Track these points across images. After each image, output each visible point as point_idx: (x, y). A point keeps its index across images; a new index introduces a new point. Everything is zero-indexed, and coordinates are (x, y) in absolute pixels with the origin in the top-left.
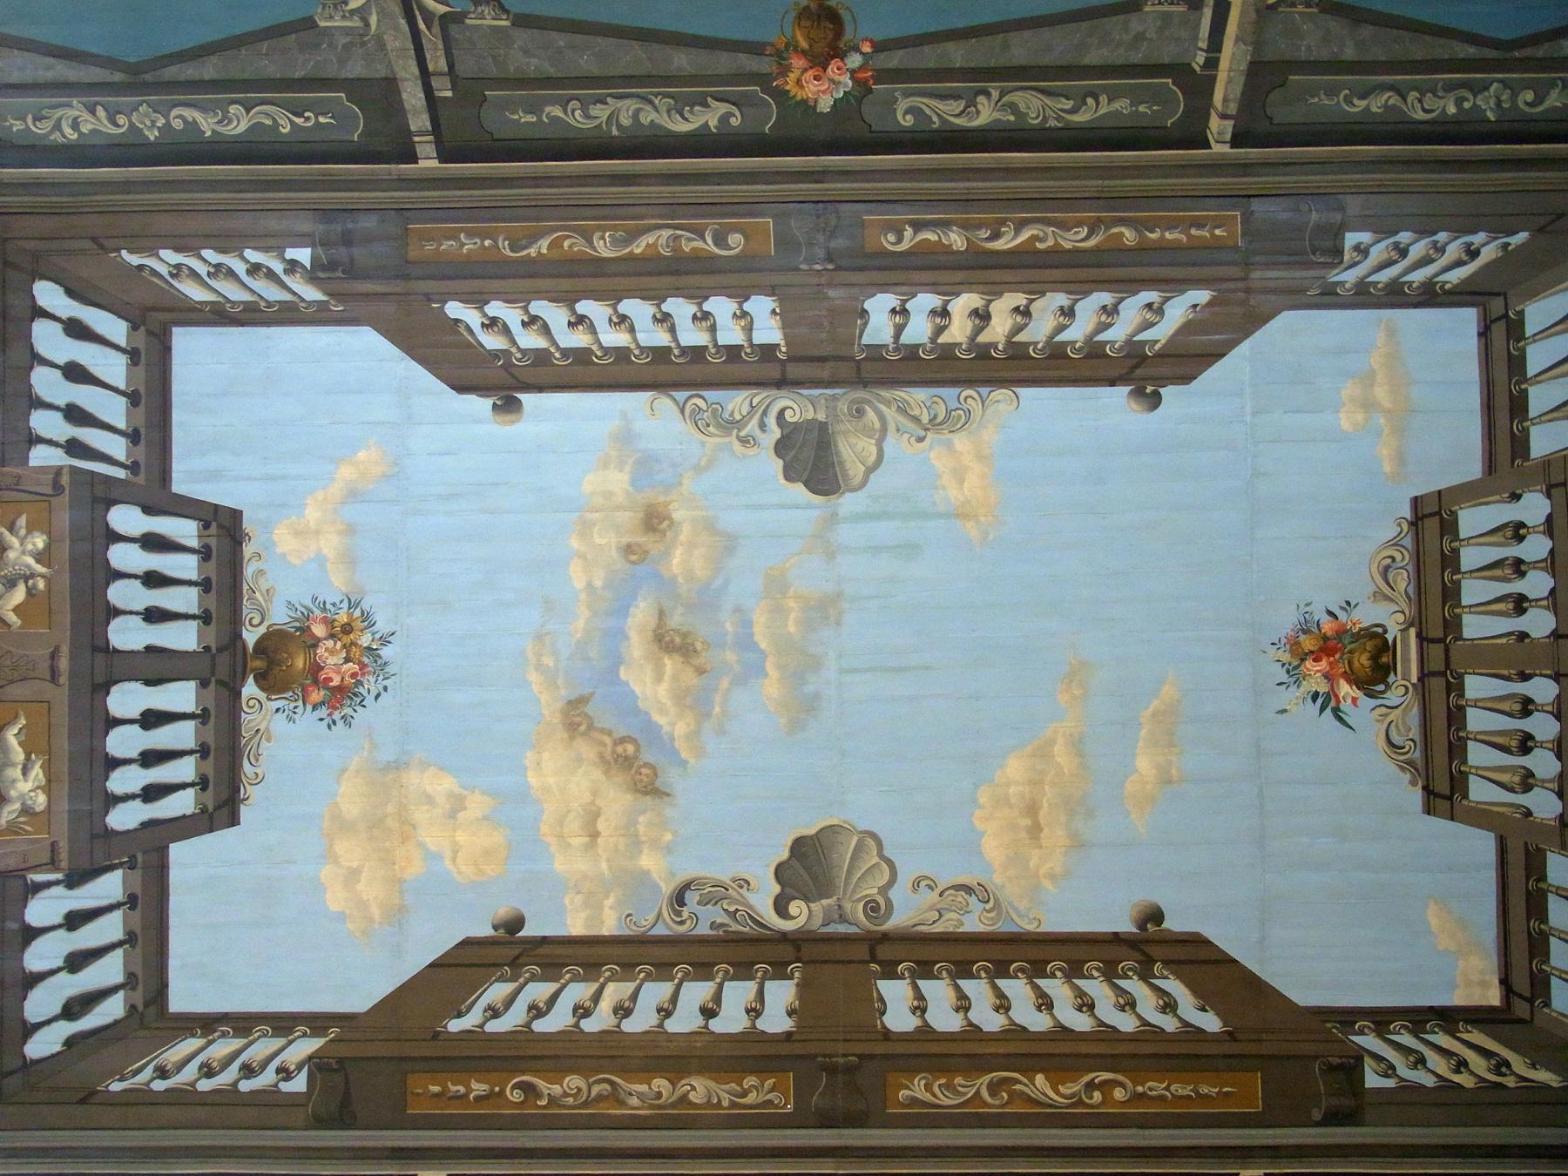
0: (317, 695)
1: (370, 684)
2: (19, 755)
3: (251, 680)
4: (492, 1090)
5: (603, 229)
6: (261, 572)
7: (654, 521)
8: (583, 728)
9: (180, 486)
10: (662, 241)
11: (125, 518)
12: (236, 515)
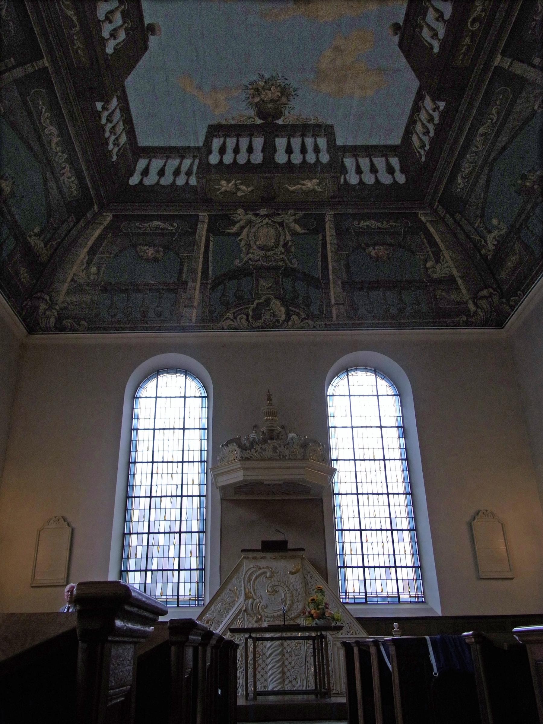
0: (284, 100)
1: (280, 82)
2: (299, 186)
3: (277, 121)
11: (214, 159)
12: (210, 127)
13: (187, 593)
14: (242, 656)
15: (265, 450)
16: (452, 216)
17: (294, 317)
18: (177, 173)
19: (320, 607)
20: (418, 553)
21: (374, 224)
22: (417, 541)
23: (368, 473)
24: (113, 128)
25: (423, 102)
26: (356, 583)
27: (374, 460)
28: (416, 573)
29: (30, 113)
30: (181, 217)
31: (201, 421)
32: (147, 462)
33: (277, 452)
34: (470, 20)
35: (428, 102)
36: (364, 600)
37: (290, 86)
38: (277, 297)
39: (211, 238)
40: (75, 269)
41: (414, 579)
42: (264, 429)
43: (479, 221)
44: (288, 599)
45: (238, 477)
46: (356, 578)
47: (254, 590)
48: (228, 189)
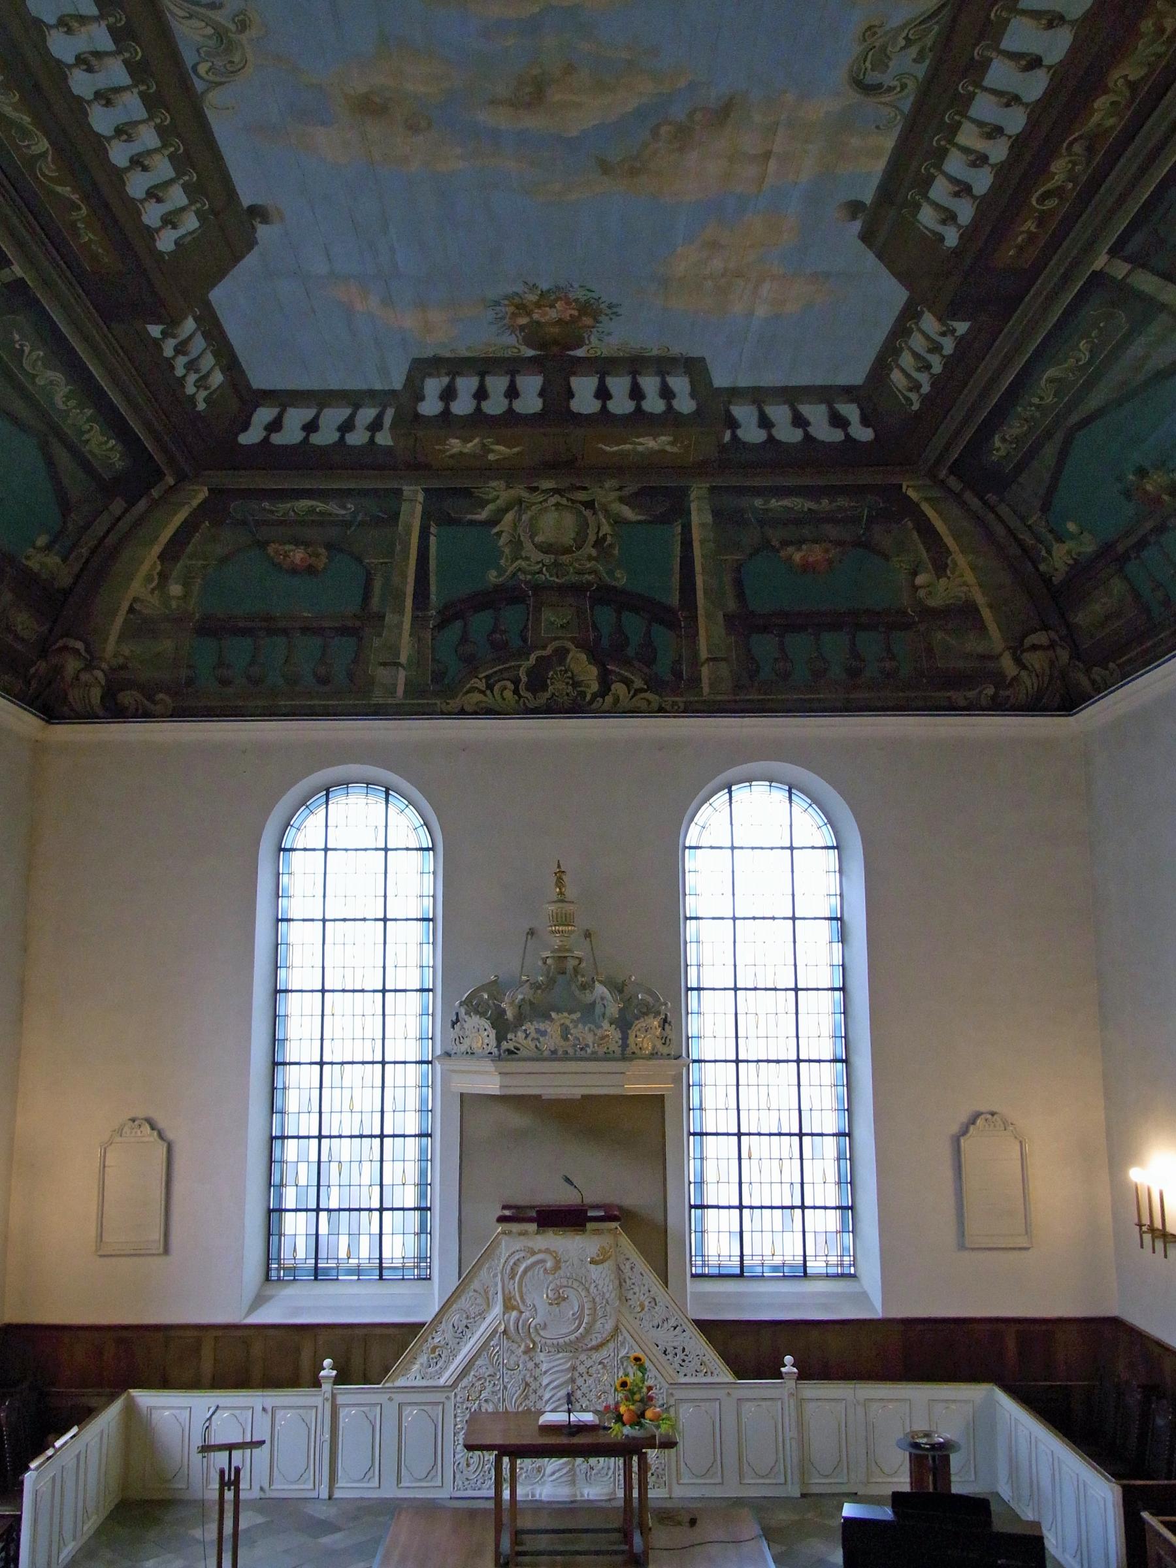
2: (628, 447)
11: (430, 406)
13: (398, 1254)
15: (544, 1033)
17: (619, 688)
19: (637, 1397)
20: (849, 1181)
22: (848, 1157)
23: (762, 1018)
26: (725, 1237)
27: (775, 989)
28: (843, 1221)
30: (364, 493)
35: (929, 323)
36: (738, 1271)
38: (581, 645)
39: (433, 530)
40: (137, 587)
44: (587, 1312)
46: (724, 1227)
47: (522, 1297)
48: (466, 450)
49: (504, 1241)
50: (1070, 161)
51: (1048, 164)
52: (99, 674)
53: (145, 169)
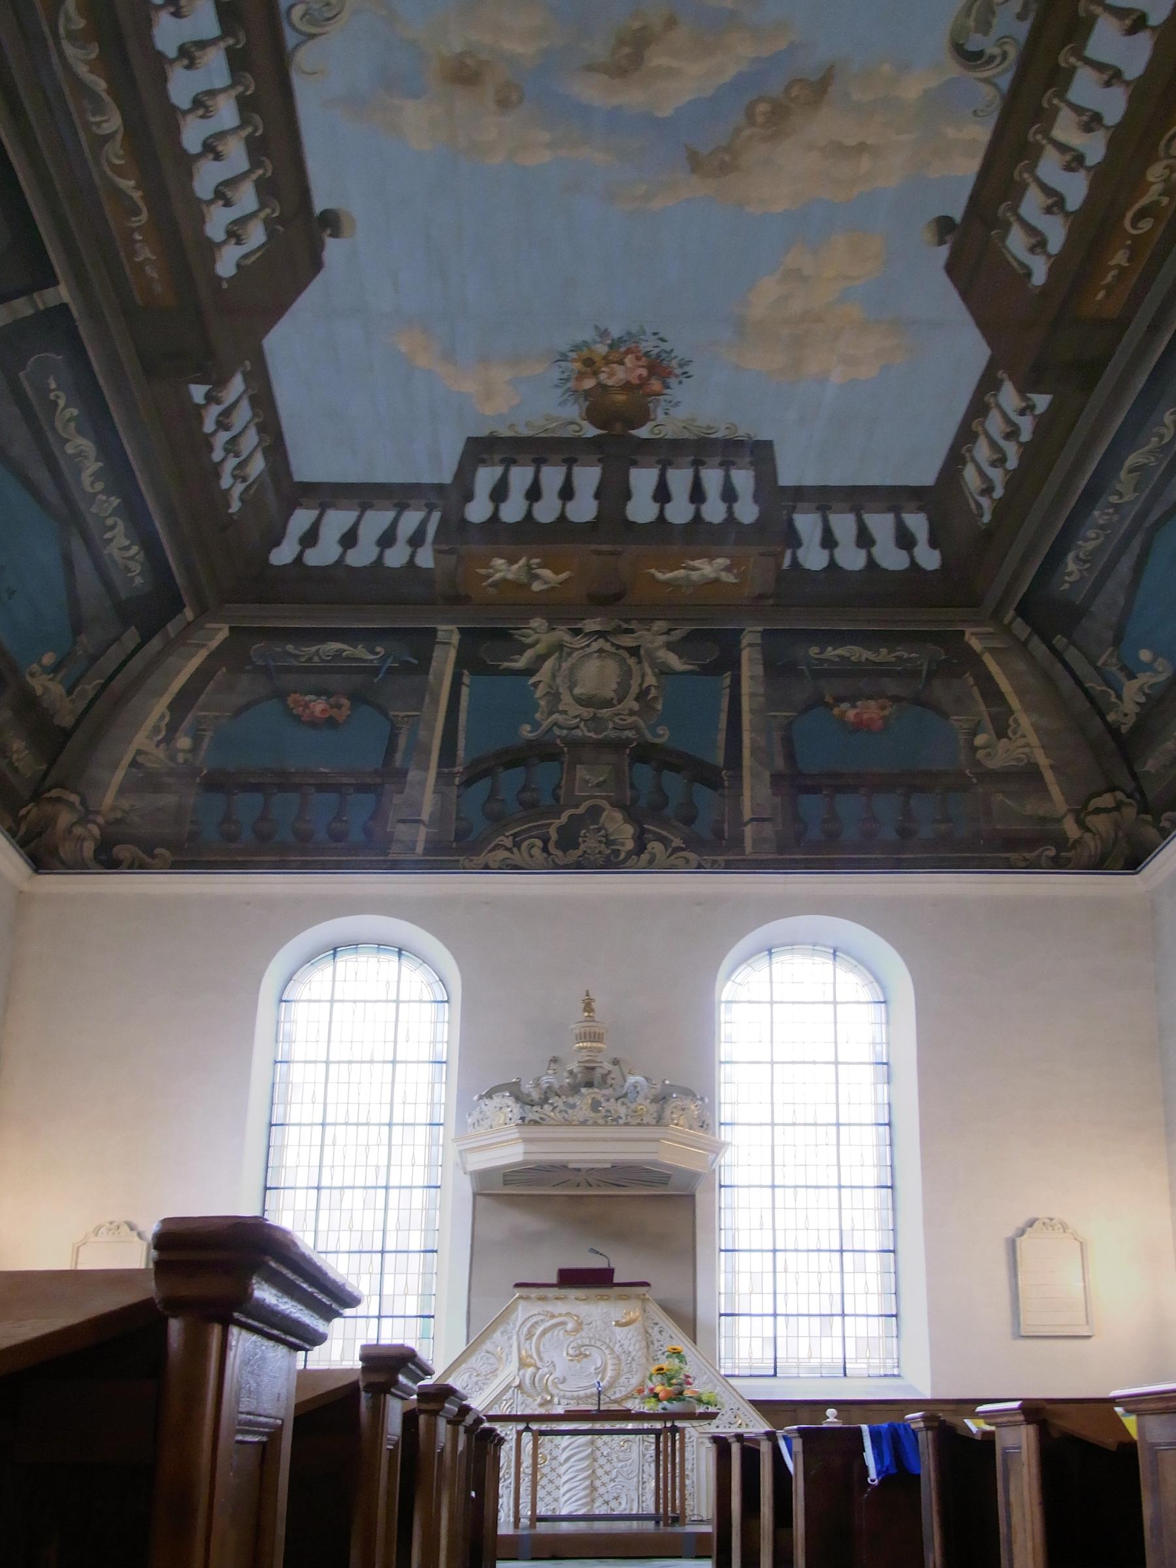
0: (655, 385)
1: (648, 345)
2: (681, 573)
3: (634, 432)
4: (1130, 247)
5: (87, 125)
6: (527, 425)
7: (464, 74)
8: (727, 158)
9: (447, 478)
10: (80, 53)
11: (478, 511)
14: (510, 1461)
15: (573, 1106)
16: (1047, 642)
17: (655, 847)
18: (387, 540)
19: (674, 1381)
21: (857, 653)
24: (234, 440)
25: (995, 395)
26: (757, 1343)
27: (815, 1124)
29: (29, 415)
31: (434, 1046)
32: (312, 1125)
33: (599, 1111)
34: (1130, 215)
35: (1008, 397)
37: (673, 355)
38: (618, 805)
39: (466, 679)
40: (141, 739)
41: (879, 1337)
42: (574, 1066)
43: (1108, 653)
45: (509, 1151)
47: (539, 1353)
48: (510, 576)
49: (522, 1305)
50: (1166, 167)
51: (1143, 172)
52: (96, 831)
53: (218, 157)
